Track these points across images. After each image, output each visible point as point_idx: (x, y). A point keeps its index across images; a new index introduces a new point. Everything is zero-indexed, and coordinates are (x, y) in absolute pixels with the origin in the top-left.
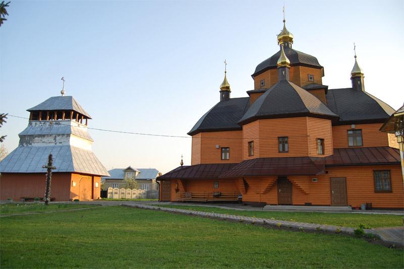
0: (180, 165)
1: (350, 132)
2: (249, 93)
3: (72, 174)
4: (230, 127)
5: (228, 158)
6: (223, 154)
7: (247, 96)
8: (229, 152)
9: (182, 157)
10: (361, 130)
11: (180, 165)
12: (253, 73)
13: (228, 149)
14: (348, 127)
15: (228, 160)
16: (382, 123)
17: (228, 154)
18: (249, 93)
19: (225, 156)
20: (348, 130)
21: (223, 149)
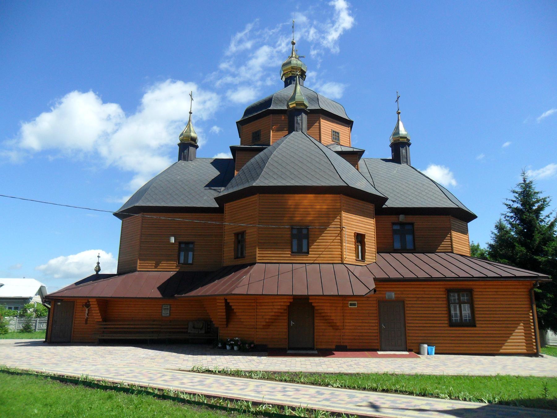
0: (95, 273)
1: (396, 227)
2: (234, 150)
3: (115, 272)
4: (384, 359)
5: (190, 261)
6: (182, 254)
7: (229, 156)
8: (193, 250)
9: (99, 257)
10: (412, 224)
11: (95, 273)
12: (240, 118)
13: (191, 246)
14: (393, 218)
15: (190, 264)
16: (162, 294)
17: (190, 254)
18: (234, 150)
19: (186, 257)
20: (394, 224)
21: (183, 246)
